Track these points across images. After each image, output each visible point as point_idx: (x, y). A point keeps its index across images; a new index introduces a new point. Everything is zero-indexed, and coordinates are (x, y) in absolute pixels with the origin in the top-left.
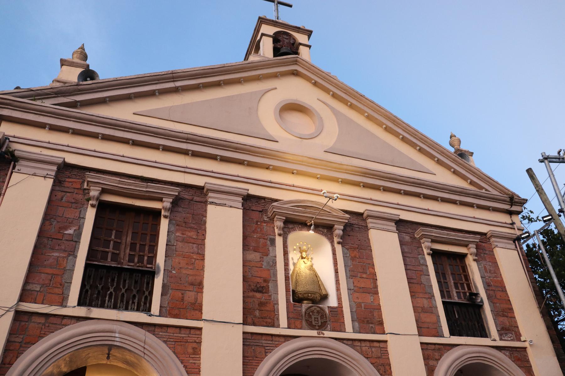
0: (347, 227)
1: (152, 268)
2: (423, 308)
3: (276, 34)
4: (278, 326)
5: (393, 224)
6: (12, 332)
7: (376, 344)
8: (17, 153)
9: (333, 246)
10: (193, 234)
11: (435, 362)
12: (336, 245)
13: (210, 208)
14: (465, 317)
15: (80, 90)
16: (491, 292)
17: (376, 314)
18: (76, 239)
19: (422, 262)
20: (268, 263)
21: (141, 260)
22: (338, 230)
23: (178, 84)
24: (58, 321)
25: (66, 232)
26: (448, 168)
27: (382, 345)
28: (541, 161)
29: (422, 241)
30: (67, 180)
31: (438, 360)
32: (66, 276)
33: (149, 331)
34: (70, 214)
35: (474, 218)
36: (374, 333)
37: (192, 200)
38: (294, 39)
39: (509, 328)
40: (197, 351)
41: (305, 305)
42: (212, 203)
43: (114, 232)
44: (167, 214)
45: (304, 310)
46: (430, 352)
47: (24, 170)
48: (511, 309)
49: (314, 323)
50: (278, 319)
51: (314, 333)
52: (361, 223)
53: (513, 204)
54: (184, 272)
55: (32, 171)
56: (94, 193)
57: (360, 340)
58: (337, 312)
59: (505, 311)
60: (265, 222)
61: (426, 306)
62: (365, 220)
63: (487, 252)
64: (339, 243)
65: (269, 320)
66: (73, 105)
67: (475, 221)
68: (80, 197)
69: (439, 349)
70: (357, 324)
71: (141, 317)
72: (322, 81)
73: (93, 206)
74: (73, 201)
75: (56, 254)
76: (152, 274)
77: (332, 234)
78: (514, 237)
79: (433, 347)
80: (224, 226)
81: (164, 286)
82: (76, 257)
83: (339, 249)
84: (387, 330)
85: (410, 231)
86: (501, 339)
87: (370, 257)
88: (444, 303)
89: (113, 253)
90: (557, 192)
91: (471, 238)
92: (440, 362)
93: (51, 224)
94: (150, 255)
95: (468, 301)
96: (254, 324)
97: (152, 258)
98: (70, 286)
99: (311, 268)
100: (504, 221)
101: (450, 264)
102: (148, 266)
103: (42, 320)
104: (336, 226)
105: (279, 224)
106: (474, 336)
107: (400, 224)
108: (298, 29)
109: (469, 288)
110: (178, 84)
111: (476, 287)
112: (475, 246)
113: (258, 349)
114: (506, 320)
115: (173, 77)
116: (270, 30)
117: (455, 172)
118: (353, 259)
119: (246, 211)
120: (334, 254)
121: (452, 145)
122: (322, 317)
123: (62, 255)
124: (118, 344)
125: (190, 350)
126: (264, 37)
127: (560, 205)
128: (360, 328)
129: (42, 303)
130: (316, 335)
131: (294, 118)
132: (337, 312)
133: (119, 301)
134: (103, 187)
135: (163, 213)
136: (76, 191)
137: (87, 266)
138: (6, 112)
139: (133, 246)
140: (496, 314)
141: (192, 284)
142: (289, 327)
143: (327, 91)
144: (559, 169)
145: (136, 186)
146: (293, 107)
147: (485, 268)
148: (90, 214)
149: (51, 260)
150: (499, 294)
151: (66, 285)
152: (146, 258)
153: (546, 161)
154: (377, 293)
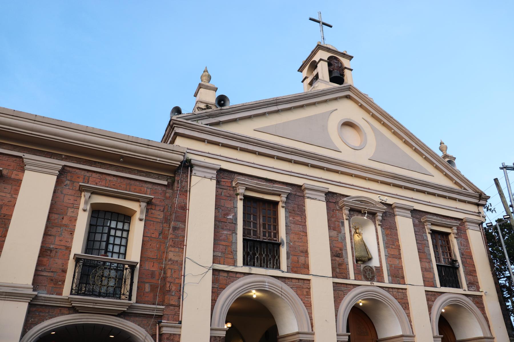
0: (385, 214)
1: (276, 240)
2: (425, 269)
3: (330, 58)
4: (349, 279)
5: (409, 212)
6: (214, 282)
7: (400, 291)
8: (192, 162)
9: (376, 226)
10: (298, 218)
11: (432, 303)
12: (378, 226)
13: (308, 202)
14: (449, 275)
15: (222, 113)
16: (464, 259)
17: (400, 272)
18: (234, 222)
19: (425, 238)
20: (341, 238)
21: (270, 236)
22: (379, 217)
23: (280, 107)
24: (234, 275)
25: (228, 217)
26: (442, 171)
27: (404, 291)
28: (501, 168)
29: (425, 224)
30: (223, 180)
31: (433, 301)
32: (233, 247)
33: (282, 281)
35: (456, 208)
36: (399, 284)
37: (295, 195)
38: (341, 63)
39: (473, 284)
40: (308, 294)
42: (308, 198)
43: (252, 216)
44: (284, 205)
45: (362, 269)
46: (429, 296)
47: (198, 173)
48: (475, 271)
49: (368, 277)
50: (349, 274)
51: (368, 283)
52: (391, 211)
53: (481, 199)
54: (297, 244)
55: (203, 174)
56: (241, 190)
57: (392, 288)
58: (379, 269)
59: (471, 272)
60: (337, 210)
61: (427, 267)
62: (393, 209)
63: (462, 232)
64: (379, 225)
65: (344, 275)
66: (218, 124)
67: (456, 210)
68: (232, 192)
69: (434, 295)
70: (390, 278)
73: (241, 199)
74: (228, 195)
75: (225, 232)
77: (375, 218)
78: (480, 222)
79: (431, 293)
80: (316, 211)
82: (236, 234)
83: (379, 228)
85: (418, 216)
86: (469, 290)
87: (396, 235)
88: (437, 265)
89: (253, 230)
90: (510, 192)
91: (454, 223)
92: (435, 303)
93: (219, 212)
94: (275, 232)
95: (451, 264)
97: (276, 234)
98: (236, 253)
99: (362, 240)
100: (473, 211)
101: (441, 238)
102: (275, 239)
103: (225, 274)
104: (378, 214)
105: (346, 212)
106: (453, 287)
107: (414, 212)
108: (344, 55)
109: (451, 256)
110: (280, 107)
111: (455, 256)
112: (456, 228)
113: (340, 293)
115: (276, 102)
117: (446, 175)
118: (387, 235)
119: (328, 202)
120: (377, 232)
121: (441, 149)
123: (229, 233)
124: (267, 289)
125: (305, 293)
126: (321, 62)
127: (511, 201)
128: (392, 280)
129: (224, 264)
130: (370, 284)
131: (349, 132)
132: (379, 269)
133: (262, 262)
134: (247, 186)
136: (229, 188)
139: (264, 225)
140: (467, 274)
143: (368, 112)
144: (510, 173)
145: (267, 187)
146: (348, 124)
147: (461, 242)
148: (240, 205)
149: (223, 237)
150: (468, 260)
151: (234, 253)
152: (272, 234)
153: (505, 169)
154: (400, 258)
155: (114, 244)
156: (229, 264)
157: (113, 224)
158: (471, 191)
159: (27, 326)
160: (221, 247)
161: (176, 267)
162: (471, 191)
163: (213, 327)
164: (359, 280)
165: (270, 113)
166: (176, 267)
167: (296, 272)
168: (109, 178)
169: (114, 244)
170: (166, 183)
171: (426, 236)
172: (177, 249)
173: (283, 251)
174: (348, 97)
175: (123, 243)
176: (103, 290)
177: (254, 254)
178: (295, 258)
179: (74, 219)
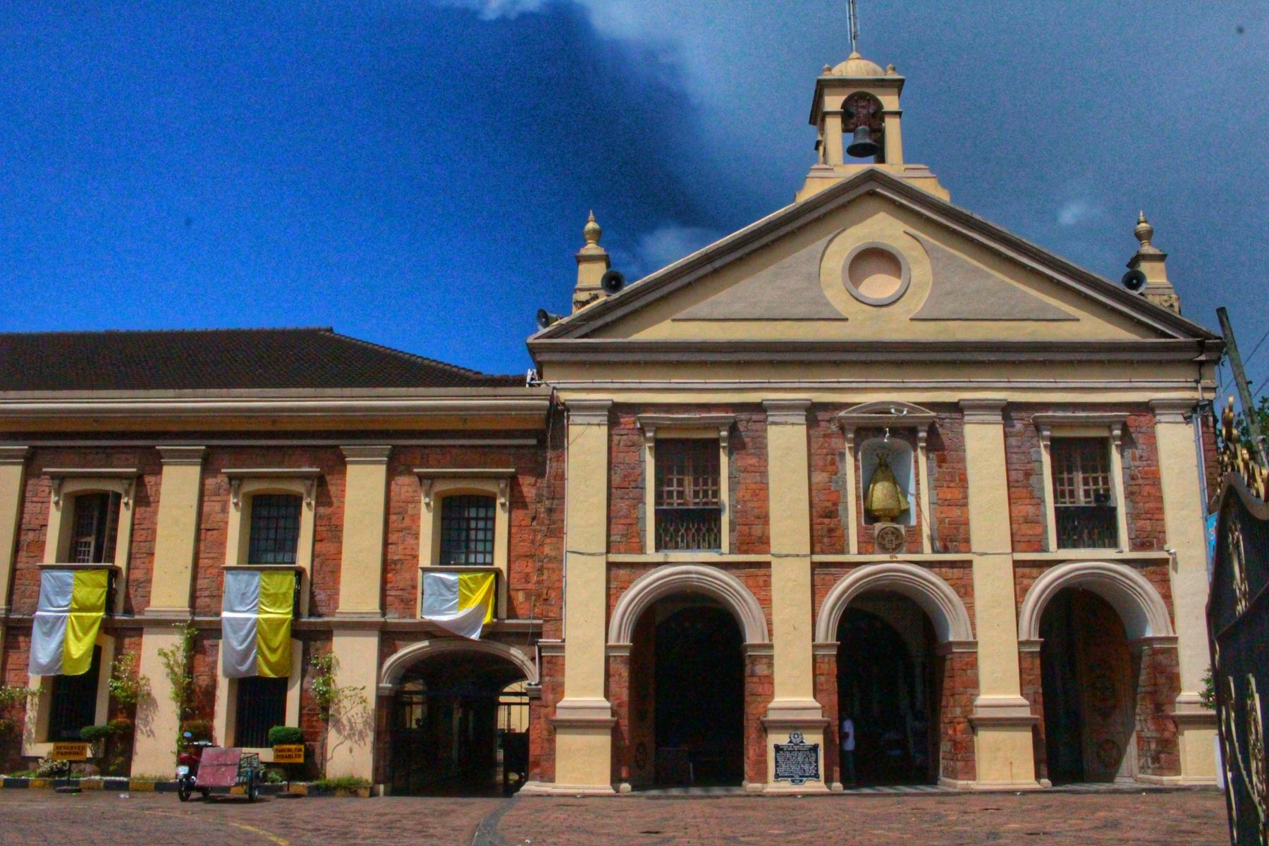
4: (922, 553)
10: (754, 461)
13: (968, 429)
17: (962, 528)
21: (705, 495)
23: (717, 264)
32: (640, 525)
34: (630, 458)
40: (767, 584)
41: (878, 526)
45: (876, 532)
51: (886, 557)
71: (712, 556)
76: (717, 513)
80: (786, 443)
96: (823, 552)
97: (716, 493)
101: (1080, 452)
110: (717, 264)
122: (897, 538)
125: (761, 583)
132: (915, 532)
137: (657, 512)
142: (859, 553)
151: (641, 535)
155: (476, 541)
157: (473, 513)
159: (382, 658)
161: (554, 565)
163: (610, 643)
164: (867, 553)
166: (554, 565)
167: (746, 552)
168: (454, 451)
169: (476, 541)
170: (533, 442)
171: (1039, 453)
172: (554, 540)
173: (725, 519)
174: (873, 194)
175: (489, 537)
177: (677, 531)
179: (416, 518)
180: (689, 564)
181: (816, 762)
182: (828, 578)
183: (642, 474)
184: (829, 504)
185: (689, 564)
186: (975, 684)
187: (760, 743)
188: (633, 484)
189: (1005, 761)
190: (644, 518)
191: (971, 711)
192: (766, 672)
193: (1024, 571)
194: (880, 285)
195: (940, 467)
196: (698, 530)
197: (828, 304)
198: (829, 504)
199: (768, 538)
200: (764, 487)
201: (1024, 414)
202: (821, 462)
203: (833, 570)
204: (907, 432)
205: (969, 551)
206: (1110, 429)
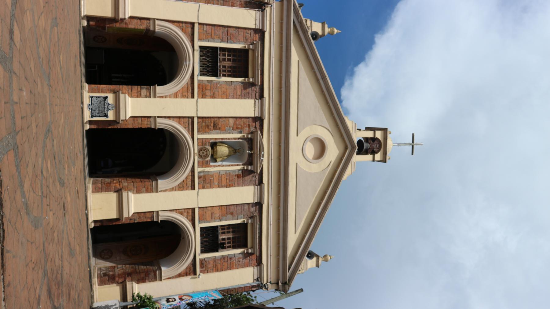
4: (198, 134)
10: (239, 93)
13: (252, 101)
17: (209, 185)
31: (187, 218)
32: (212, 40)
34: (241, 37)
37: (256, 91)
39: (206, 267)
40: (184, 97)
45: (207, 147)
51: (196, 151)
72: (342, 164)
76: (216, 75)
80: (246, 108)
81: (212, 81)
84: (200, 191)
101: (240, 236)
108: (385, 153)
114: (211, 266)
116: (379, 135)
122: (205, 156)
125: (184, 94)
135: (246, 79)
137: (217, 48)
138: (285, 2)
141: (214, 93)
142: (198, 139)
151: (206, 39)
154: (219, 187)
156: (199, 35)
158: (288, 274)
160: (210, 30)
162: (288, 274)
163: (156, 21)
164: (198, 143)
165: (314, 73)
167: (199, 87)
171: (241, 219)
174: (346, 148)
176: (149, 123)
178: (209, 88)
180: (193, 61)
181: (99, 116)
182: (187, 124)
183: (234, 42)
184: (220, 126)
185: (193, 61)
186: (138, 192)
187: (108, 90)
188: (229, 38)
189: (102, 206)
190: (214, 42)
191: (126, 190)
192: (143, 94)
193: (189, 27)
194: (311, 150)
195: (235, 175)
196: (208, 67)
197: (304, 128)
198: (220, 126)
199: (205, 98)
200: (227, 97)
201: (257, 212)
202: (238, 122)
203: (190, 127)
204: (250, 161)
205: (199, 188)
206: (252, 248)
